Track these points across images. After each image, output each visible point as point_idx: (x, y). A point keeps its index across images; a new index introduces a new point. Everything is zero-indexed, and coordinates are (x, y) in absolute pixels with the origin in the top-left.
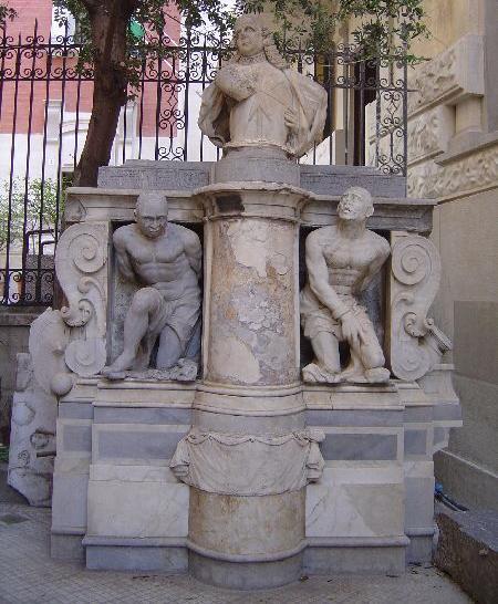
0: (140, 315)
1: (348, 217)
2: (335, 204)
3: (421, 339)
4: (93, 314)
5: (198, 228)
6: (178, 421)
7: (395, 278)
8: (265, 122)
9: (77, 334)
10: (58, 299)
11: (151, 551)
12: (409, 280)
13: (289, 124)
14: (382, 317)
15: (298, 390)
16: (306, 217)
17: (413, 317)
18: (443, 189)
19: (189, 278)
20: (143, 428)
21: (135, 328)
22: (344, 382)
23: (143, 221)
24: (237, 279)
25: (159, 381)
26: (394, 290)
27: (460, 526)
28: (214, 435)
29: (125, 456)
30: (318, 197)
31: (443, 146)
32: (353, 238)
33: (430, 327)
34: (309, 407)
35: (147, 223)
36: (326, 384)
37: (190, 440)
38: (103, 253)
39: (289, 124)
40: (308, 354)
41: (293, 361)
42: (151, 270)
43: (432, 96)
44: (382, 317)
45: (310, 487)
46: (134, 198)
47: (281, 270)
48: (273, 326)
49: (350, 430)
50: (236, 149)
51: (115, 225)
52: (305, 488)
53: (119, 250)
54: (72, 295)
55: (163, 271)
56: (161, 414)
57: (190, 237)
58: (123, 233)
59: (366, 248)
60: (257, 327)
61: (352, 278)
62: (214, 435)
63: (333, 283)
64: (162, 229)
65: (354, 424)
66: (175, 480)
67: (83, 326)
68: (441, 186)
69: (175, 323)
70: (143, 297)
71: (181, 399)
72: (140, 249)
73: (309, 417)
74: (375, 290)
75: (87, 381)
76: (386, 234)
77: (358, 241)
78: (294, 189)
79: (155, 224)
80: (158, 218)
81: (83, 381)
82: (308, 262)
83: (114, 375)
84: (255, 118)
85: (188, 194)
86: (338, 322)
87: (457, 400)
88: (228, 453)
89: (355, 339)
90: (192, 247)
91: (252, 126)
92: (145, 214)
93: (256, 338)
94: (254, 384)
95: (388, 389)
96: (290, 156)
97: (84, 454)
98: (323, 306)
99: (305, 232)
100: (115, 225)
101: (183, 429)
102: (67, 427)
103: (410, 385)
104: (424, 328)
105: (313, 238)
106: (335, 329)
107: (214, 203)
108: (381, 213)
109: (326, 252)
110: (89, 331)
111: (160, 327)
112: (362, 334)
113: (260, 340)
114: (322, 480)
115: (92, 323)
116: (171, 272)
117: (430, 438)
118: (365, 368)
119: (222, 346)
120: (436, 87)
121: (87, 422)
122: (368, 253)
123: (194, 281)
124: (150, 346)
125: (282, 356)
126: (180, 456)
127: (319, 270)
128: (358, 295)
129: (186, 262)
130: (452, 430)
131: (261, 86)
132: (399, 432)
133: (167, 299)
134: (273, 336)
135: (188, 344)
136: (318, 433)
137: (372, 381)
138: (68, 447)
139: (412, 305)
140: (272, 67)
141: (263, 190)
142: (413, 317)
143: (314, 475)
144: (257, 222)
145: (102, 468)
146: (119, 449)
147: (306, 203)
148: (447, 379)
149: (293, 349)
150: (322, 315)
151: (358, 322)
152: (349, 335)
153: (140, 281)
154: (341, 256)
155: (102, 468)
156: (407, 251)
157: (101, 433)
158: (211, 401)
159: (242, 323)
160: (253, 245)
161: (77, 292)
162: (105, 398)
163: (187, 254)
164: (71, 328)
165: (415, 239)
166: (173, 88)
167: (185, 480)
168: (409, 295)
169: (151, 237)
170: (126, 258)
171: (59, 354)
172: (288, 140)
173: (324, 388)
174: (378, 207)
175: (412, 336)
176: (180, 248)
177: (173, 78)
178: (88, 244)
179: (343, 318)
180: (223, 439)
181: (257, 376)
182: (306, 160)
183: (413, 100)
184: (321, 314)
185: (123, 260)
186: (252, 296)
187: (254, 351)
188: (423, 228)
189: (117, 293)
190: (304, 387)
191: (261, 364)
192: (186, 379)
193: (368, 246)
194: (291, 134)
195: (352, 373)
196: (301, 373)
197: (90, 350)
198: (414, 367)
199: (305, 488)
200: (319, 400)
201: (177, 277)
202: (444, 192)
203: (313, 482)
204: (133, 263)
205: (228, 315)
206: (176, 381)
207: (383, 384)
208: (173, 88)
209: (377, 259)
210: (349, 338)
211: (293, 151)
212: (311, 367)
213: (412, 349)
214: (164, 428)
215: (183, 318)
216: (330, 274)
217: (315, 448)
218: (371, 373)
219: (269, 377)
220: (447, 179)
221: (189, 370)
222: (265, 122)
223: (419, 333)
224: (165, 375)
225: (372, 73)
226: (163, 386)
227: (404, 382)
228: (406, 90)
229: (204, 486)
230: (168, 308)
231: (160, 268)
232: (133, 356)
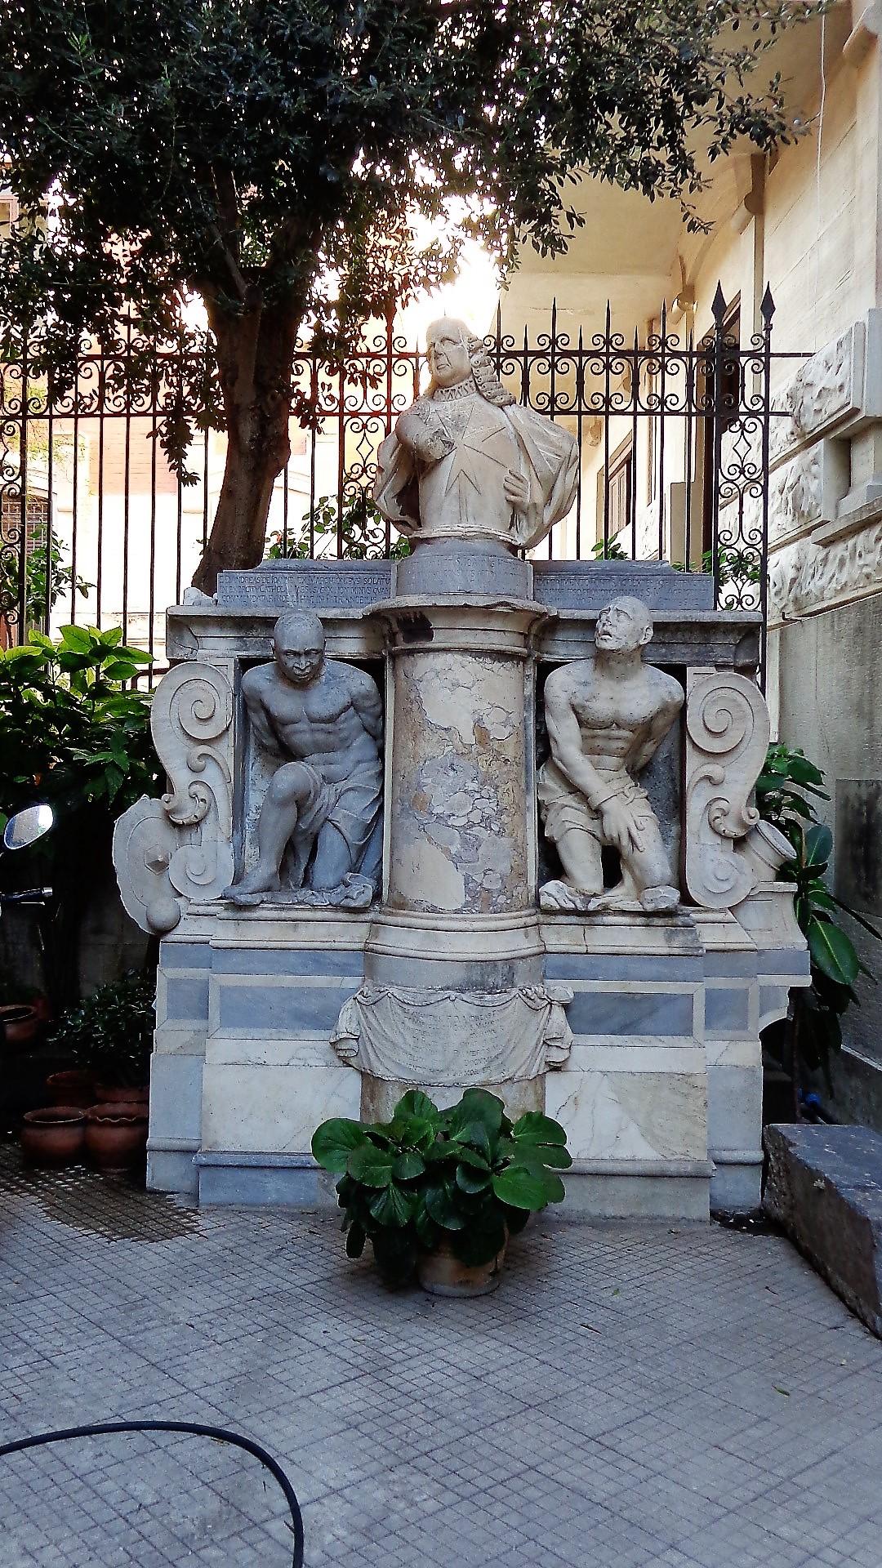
0: (283, 804)
1: (609, 644)
2: (591, 625)
3: (739, 843)
4: (210, 806)
5: (373, 667)
6: (344, 970)
7: (694, 745)
8: (472, 495)
9: (191, 836)
10: (162, 786)
11: (301, 1174)
12: (715, 746)
13: (512, 498)
14: (673, 809)
15: (534, 920)
16: (548, 645)
17: (722, 804)
18: (823, 589)
19: (361, 744)
20: (288, 980)
21: (281, 823)
22: (605, 910)
23: (284, 658)
24: (428, 747)
25: (314, 908)
26: (693, 762)
27: (792, 1145)
28: (394, 990)
29: (262, 1025)
30: (565, 614)
31: (824, 512)
32: (621, 678)
33: (753, 822)
34: (549, 948)
35: (291, 662)
36: (575, 912)
37: (360, 997)
38: (224, 711)
39: (512, 498)
40: (552, 865)
41: (523, 875)
42: (301, 735)
43: (812, 422)
44: (673, 809)
45: (551, 1078)
46: (269, 623)
47: (498, 732)
48: (486, 821)
49: (615, 987)
50: (427, 540)
51: (245, 664)
52: (541, 1077)
53: (252, 704)
54: (179, 776)
55: (320, 737)
56: (316, 959)
57: (363, 681)
58: (258, 678)
59: (642, 694)
60: (462, 822)
61: (621, 744)
62: (394, 990)
63: (590, 750)
64: (316, 672)
65: (625, 976)
66: (339, 1063)
67: (196, 825)
68: (820, 583)
69: (338, 816)
70: (290, 776)
71: (349, 935)
72: (283, 703)
73: (547, 963)
74: (658, 758)
75: (201, 910)
76: (679, 672)
77: (627, 684)
78: (519, 603)
79: (303, 662)
80: (307, 653)
81: (195, 909)
82: (549, 719)
83: (243, 899)
84: (455, 490)
85: (357, 613)
86: (597, 813)
87: (801, 941)
88: (414, 1018)
89: (625, 841)
90: (366, 697)
91: (450, 506)
92: (286, 648)
93: (458, 841)
94: (456, 912)
95: (679, 920)
96: (513, 549)
97: (198, 1024)
98: (575, 790)
99: (545, 670)
100: (245, 664)
101: (351, 982)
102: (173, 983)
103: (719, 916)
104: (744, 825)
105: (556, 678)
106: (593, 826)
107: (395, 627)
108: (667, 638)
109: (575, 702)
110: (207, 829)
111: (318, 824)
112: (634, 832)
113: (465, 842)
114: (571, 1065)
115: (211, 816)
116: (332, 738)
117: (754, 1004)
118: (641, 886)
119: (408, 852)
120: (817, 406)
121: (202, 973)
122: (645, 702)
123: (372, 752)
124: (297, 856)
125: (504, 867)
126: (347, 1021)
127: (566, 733)
128: (640, 773)
129: (356, 720)
130: (795, 993)
131: (468, 438)
132: (698, 991)
133: (328, 780)
134: (485, 834)
135: (362, 850)
136: (564, 990)
137: (649, 907)
138: (174, 1014)
139: (724, 787)
140: (482, 401)
141: (466, 606)
142: (722, 804)
143: (557, 1056)
144: (458, 657)
145: (224, 1047)
146: (249, 1014)
147: (544, 628)
148: (789, 901)
149: (523, 856)
150: (574, 804)
151: (631, 813)
152: (615, 835)
153: (284, 752)
154: (601, 708)
155: (224, 1047)
156: (709, 693)
157: (223, 990)
158: (396, 940)
159: (439, 817)
160: (460, 694)
161: (186, 771)
162: (224, 934)
163: (357, 710)
164: (179, 827)
165: (730, 678)
166: (365, 426)
167: (353, 1062)
168: (715, 769)
169: (300, 683)
170: (263, 714)
171: (160, 866)
172: (512, 525)
173: (574, 919)
174: (658, 627)
175: (724, 837)
176: (346, 699)
177: (365, 409)
178: (201, 695)
179: (605, 807)
180: (408, 998)
181: (459, 898)
182: (539, 553)
183: (781, 429)
184: (570, 800)
185: (258, 719)
186: (452, 773)
187: (457, 860)
188: (743, 661)
189: (252, 773)
190: (542, 918)
191: (467, 880)
192: (353, 904)
193: (645, 691)
194: (517, 511)
195: (621, 896)
196: (537, 897)
197: (208, 860)
198: (726, 887)
199: (541, 1077)
200: (561, 938)
201: (345, 745)
202: (827, 594)
203: (556, 1068)
204: (275, 725)
205: (415, 803)
206: (337, 908)
207: (668, 913)
208: (365, 426)
209: (662, 711)
210: (616, 841)
211: (520, 541)
212: (552, 886)
213: (723, 858)
214: (320, 981)
215: (350, 812)
216: (584, 738)
217: (559, 1014)
218: (648, 894)
219: (479, 899)
220: (832, 567)
221: (361, 891)
222: (472, 495)
223: (735, 831)
224: (323, 900)
225: (732, 384)
226: (319, 915)
227: (708, 910)
228: (767, 414)
229: (380, 1071)
230: (328, 793)
231: (312, 730)
232: (274, 868)
